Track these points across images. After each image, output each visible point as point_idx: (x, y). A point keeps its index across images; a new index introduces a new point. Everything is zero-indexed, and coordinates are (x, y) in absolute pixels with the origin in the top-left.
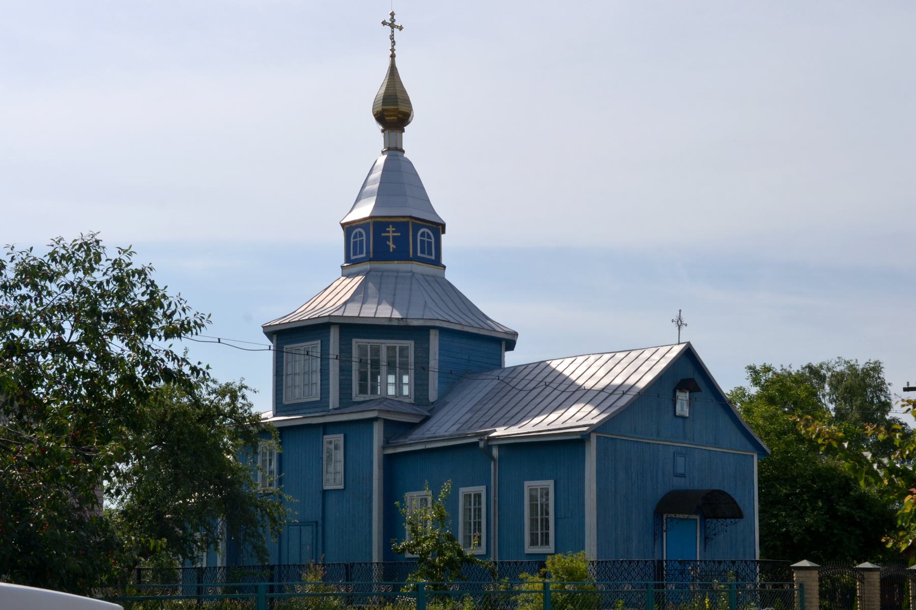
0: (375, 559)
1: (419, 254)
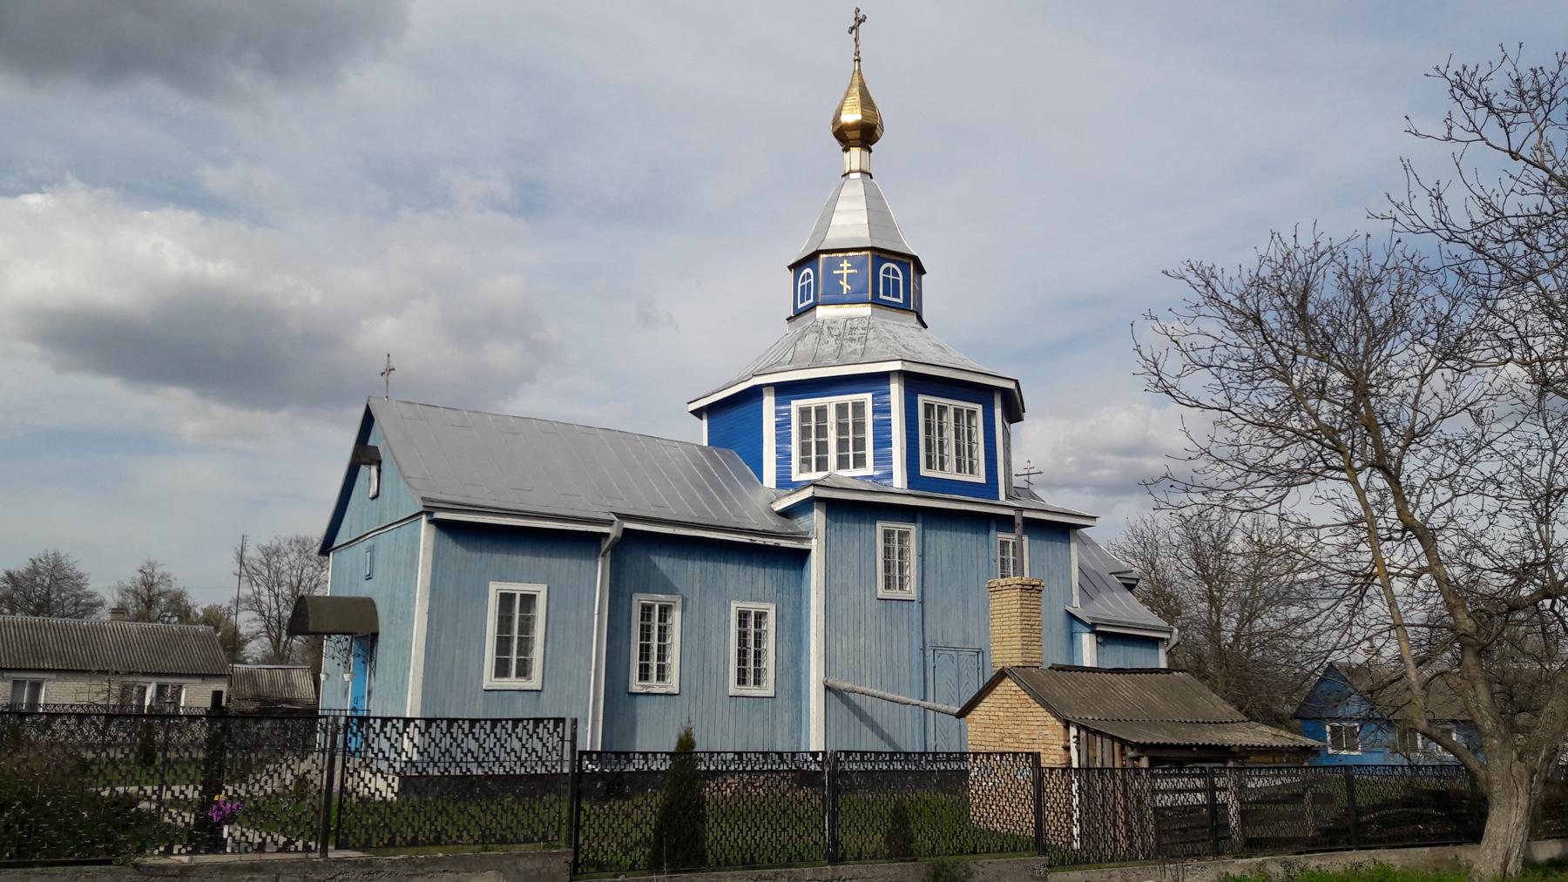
0: (25, 701)
1: (882, 296)
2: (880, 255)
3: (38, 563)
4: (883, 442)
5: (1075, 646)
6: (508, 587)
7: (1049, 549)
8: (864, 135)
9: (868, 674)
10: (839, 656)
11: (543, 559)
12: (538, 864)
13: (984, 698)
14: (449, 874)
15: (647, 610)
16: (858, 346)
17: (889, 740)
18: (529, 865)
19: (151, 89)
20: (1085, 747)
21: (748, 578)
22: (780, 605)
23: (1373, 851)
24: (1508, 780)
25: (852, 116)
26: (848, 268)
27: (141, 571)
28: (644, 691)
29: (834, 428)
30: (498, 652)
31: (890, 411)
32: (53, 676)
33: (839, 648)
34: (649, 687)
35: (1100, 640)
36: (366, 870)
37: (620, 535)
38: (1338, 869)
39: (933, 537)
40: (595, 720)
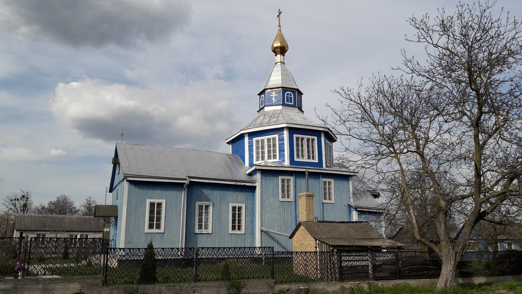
1: (286, 103)
2: (285, 89)
3: (59, 199)
4: (282, 150)
5: (351, 215)
6: (152, 201)
7: (342, 184)
8: (282, 50)
9: (276, 226)
10: (266, 220)
11: (164, 192)
12: (92, 281)
13: (296, 232)
14: (62, 283)
15: (201, 207)
16: (275, 119)
17: (284, 248)
18: (89, 281)
19: (113, 47)
20: (320, 246)
21: (236, 196)
22: (247, 204)
23: (405, 280)
24: (448, 256)
25: (277, 44)
26: (275, 94)
27: (87, 200)
28: (200, 233)
29: (267, 146)
30: (150, 221)
31: (284, 140)
32: (49, 232)
33: (266, 218)
34: (202, 231)
35: (359, 213)
36: (36, 282)
37: (188, 183)
38: (391, 285)
39: (299, 181)
40: (182, 242)
